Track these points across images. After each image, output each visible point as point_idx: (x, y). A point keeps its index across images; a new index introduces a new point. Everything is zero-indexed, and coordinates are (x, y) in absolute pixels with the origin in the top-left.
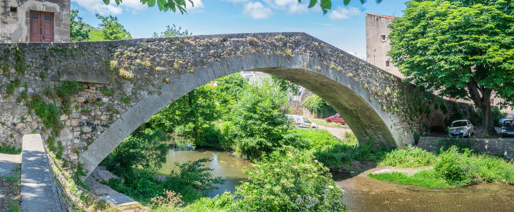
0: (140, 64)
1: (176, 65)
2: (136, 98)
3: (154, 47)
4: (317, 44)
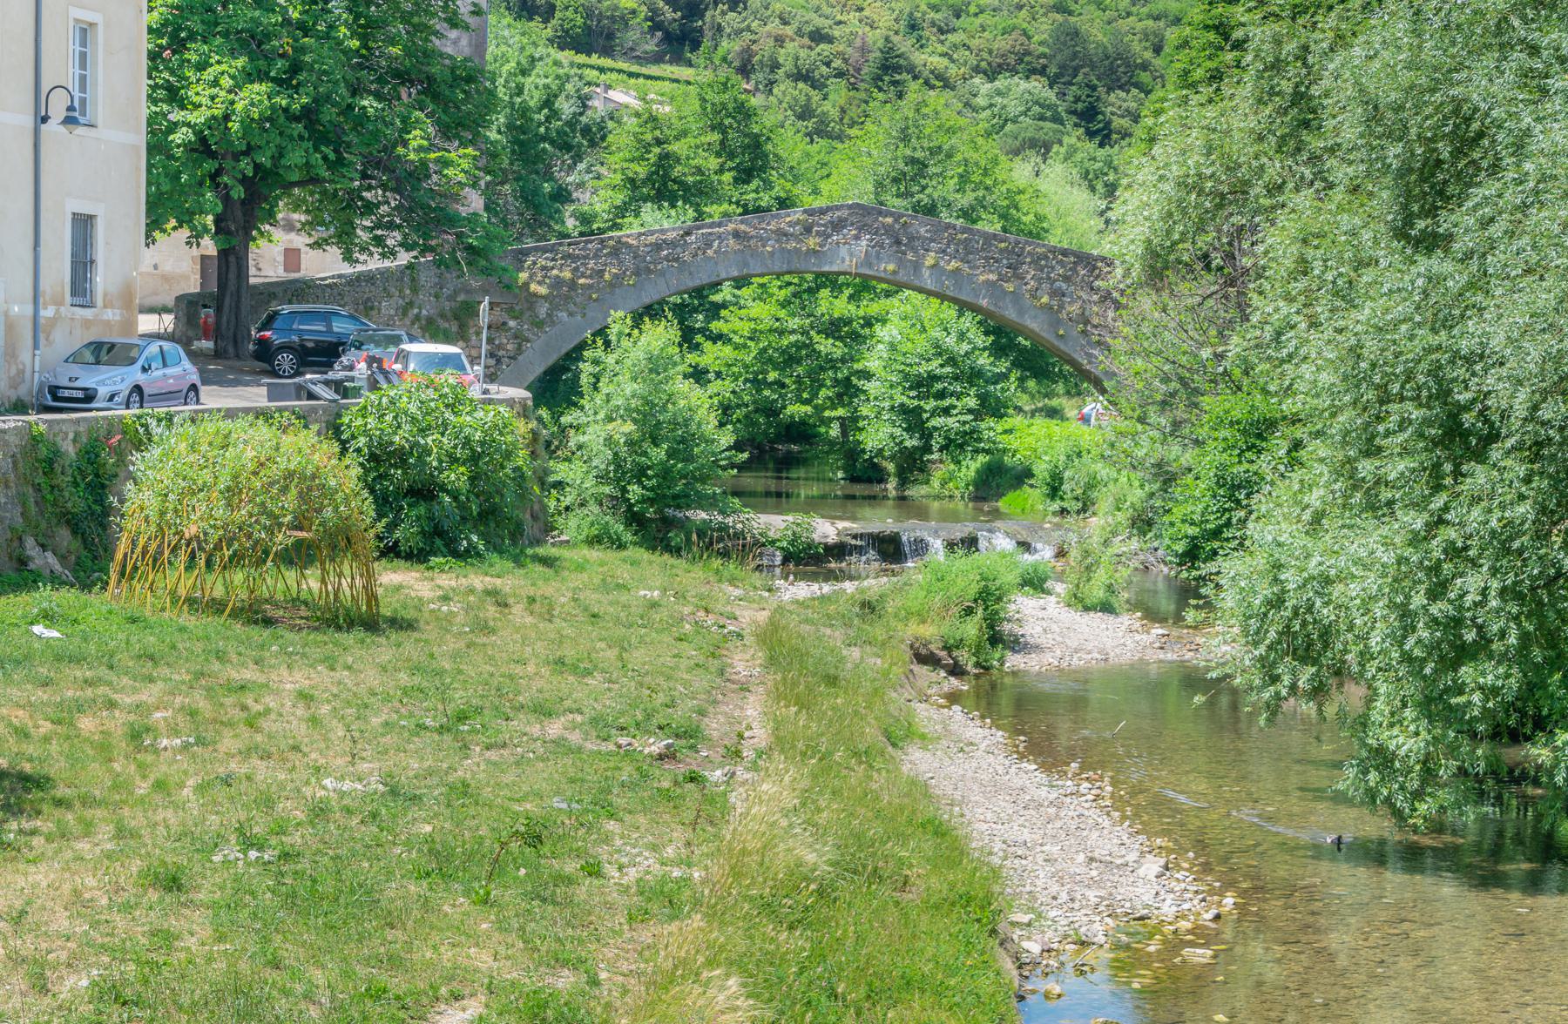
0: (558, 277)
1: (607, 276)
2: (553, 322)
3: (577, 252)
4: (889, 220)
